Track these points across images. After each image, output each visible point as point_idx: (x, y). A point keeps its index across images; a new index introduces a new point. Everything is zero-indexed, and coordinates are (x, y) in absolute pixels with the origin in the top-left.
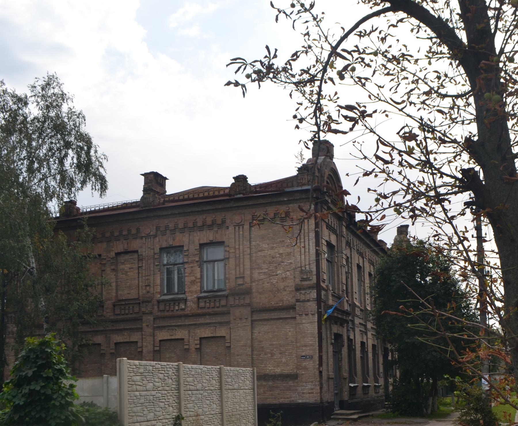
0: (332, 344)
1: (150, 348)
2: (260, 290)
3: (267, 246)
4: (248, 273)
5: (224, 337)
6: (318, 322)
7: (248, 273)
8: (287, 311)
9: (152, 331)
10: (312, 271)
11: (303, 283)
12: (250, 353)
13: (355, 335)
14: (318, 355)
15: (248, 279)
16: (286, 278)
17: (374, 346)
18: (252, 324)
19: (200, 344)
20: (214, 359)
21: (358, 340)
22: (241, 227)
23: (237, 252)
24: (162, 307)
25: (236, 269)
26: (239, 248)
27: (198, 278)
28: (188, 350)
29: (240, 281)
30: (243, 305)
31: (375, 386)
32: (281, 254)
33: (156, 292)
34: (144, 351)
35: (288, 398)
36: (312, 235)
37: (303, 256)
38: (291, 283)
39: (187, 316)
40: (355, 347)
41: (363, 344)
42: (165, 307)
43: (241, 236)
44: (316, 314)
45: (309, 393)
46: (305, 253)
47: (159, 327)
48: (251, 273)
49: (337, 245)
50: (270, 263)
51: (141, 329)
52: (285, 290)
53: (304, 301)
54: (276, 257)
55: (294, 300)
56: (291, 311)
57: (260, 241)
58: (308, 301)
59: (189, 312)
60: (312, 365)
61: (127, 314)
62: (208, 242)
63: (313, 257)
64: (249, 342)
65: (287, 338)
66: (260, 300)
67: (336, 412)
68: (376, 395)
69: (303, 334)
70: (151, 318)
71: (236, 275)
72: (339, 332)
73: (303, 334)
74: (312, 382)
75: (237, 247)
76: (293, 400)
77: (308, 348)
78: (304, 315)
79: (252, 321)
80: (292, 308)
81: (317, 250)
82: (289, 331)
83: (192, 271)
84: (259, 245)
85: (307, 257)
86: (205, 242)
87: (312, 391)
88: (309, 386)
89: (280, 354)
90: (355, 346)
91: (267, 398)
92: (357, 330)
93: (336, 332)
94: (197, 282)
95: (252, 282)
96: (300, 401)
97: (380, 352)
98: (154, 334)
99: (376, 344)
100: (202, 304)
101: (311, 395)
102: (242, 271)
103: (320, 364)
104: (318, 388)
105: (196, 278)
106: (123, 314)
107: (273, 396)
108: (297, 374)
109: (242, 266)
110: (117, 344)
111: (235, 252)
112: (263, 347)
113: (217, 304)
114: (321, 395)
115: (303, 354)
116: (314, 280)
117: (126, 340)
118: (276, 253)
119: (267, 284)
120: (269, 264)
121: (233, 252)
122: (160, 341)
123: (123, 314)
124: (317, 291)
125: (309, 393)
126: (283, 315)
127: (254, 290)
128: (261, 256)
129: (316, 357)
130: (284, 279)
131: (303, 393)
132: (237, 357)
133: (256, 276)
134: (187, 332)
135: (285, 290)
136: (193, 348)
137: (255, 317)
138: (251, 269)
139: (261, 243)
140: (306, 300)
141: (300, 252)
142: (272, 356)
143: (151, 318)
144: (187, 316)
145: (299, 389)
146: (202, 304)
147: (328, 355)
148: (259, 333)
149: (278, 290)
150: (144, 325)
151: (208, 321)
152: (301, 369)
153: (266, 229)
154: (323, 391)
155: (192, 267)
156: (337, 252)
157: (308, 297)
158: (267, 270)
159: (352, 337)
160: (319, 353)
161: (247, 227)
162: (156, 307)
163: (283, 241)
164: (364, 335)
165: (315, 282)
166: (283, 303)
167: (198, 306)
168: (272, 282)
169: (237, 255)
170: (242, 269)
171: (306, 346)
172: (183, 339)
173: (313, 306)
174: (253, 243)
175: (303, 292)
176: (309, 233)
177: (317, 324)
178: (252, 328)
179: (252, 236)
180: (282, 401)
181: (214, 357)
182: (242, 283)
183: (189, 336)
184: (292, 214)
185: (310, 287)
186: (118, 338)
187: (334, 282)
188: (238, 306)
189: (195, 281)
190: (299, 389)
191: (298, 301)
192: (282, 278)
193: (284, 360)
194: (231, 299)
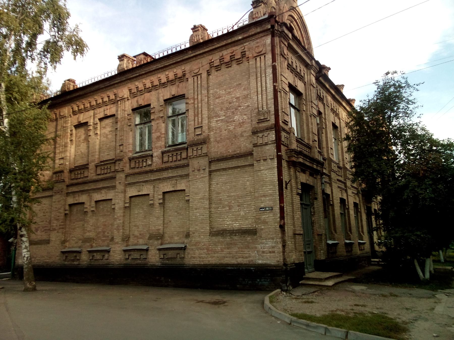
0: (298, 194)
1: (121, 204)
2: (218, 139)
3: (224, 92)
4: (205, 122)
5: (184, 190)
6: (278, 167)
7: (205, 122)
8: (243, 159)
9: (123, 188)
10: (269, 111)
11: (260, 125)
12: (207, 206)
13: (332, 190)
14: (278, 206)
15: (205, 128)
16: (243, 122)
17: (356, 205)
18: (210, 175)
19: (164, 199)
20: (176, 214)
21: (337, 195)
22: (199, 77)
23: (196, 102)
24: (133, 165)
25: (194, 119)
26: (198, 99)
27: (163, 134)
28: (152, 205)
29: (198, 132)
30: (200, 156)
31: (360, 244)
32: (238, 98)
33: (129, 151)
34: (116, 208)
35: (246, 258)
36: (270, 71)
37: (260, 96)
38: (248, 128)
39: (152, 171)
40: (333, 203)
41: (342, 201)
42: (135, 164)
43: (199, 86)
44: (276, 159)
45: (270, 252)
46: (262, 92)
47: (129, 184)
48: (209, 122)
49: (306, 94)
50: (227, 109)
51: (114, 187)
52: (243, 136)
53: (262, 145)
54: (233, 102)
55: (250, 146)
56: (249, 157)
57: (217, 88)
58: (266, 144)
59: (154, 168)
60: (273, 218)
61: (106, 174)
62: (171, 97)
63: (271, 95)
64: (207, 194)
65: (245, 189)
66: (216, 149)
67: (307, 275)
68: (361, 252)
69: (262, 183)
70: (122, 175)
71: (195, 125)
72: (308, 182)
73: (262, 183)
74: (273, 239)
75: (196, 97)
76: (252, 260)
77: (268, 198)
78: (262, 161)
79: (210, 172)
80: (251, 154)
81: (274, 87)
82: (248, 180)
83: (158, 127)
84: (216, 92)
85: (264, 97)
86: (168, 97)
87: (273, 250)
88: (270, 243)
89: (239, 206)
90: (333, 201)
91: (224, 257)
92: (335, 185)
93: (304, 181)
94: (162, 138)
95: (210, 132)
96: (260, 262)
97: (363, 210)
98: (125, 191)
99: (358, 202)
100: (166, 159)
101: (272, 254)
102: (200, 121)
103: (282, 217)
104: (280, 246)
105: (161, 134)
106: (103, 174)
107: (231, 255)
108: (256, 229)
109: (200, 115)
110: (96, 202)
111: (194, 103)
112: (220, 200)
113: (179, 157)
114: (284, 254)
115: (262, 206)
116: (273, 121)
117: (103, 198)
118: (232, 98)
119: (225, 132)
120: (227, 110)
121: (192, 103)
122: (131, 197)
123: (103, 174)
124: (276, 132)
125: (270, 252)
126: (241, 162)
127: (212, 140)
128: (218, 103)
129: (277, 209)
130: (241, 124)
131: (263, 252)
132: (195, 211)
133: (213, 124)
134: (152, 187)
135: (243, 136)
136: (157, 202)
137: (213, 168)
138: (209, 118)
139: (218, 90)
140: (264, 143)
141: (257, 92)
142: (230, 209)
143: (122, 175)
144: (152, 171)
145: (259, 246)
146: (166, 159)
147: (293, 206)
148: (217, 184)
149: (235, 137)
150: (117, 182)
151: (170, 175)
152: (260, 223)
153: (222, 76)
154: (286, 249)
155: (158, 124)
156: (306, 100)
157: (266, 140)
158: (224, 117)
159: (328, 191)
160: (280, 203)
161: (204, 75)
162: (128, 165)
163: (240, 84)
164: (344, 192)
165: (274, 122)
166: (241, 150)
167: (163, 161)
168: (229, 129)
169: (196, 106)
170: (200, 119)
171: (264, 196)
172: (148, 195)
173: (271, 149)
174: (211, 92)
175: (260, 135)
176: (265, 69)
177: (276, 170)
178: (210, 179)
179: (211, 84)
180: (240, 260)
181: (176, 212)
182: (200, 133)
183: (154, 191)
184: (247, 53)
185: (268, 129)
186: (97, 196)
187: (303, 131)
188: (197, 157)
189: (160, 136)
190: (259, 246)
191: (255, 145)
192: (239, 123)
193: (242, 213)
194: (190, 150)
